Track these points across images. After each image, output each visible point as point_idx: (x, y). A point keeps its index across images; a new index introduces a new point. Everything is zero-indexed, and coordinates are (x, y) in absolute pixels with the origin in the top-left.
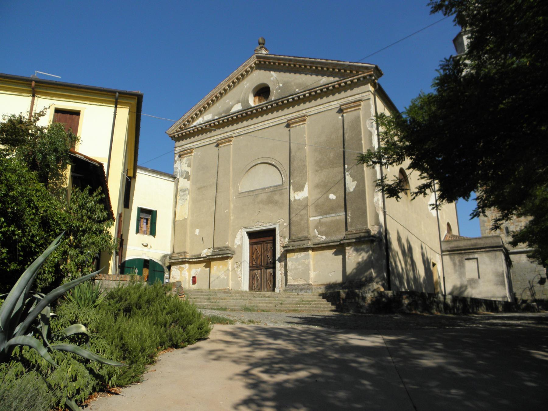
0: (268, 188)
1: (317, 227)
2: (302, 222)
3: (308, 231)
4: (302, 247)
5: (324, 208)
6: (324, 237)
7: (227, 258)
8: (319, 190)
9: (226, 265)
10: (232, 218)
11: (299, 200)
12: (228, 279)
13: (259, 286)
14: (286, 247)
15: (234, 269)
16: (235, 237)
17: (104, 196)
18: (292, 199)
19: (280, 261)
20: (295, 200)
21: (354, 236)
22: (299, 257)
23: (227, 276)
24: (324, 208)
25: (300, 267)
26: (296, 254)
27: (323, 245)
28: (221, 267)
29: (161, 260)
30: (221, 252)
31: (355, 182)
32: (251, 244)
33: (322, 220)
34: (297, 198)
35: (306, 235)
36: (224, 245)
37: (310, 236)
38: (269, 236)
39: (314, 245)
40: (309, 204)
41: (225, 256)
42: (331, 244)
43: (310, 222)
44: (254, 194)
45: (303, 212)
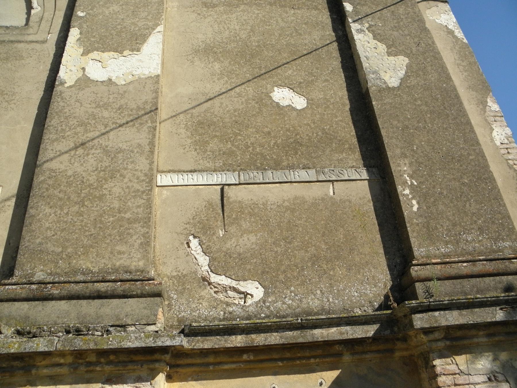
1: (201, 229)
3: (146, 243)
4: (115, 341)
5: (235, 141)
6: (256, 290)
8: (217, 66)
14: (78, 332)
18: (67, 74)
20: (84, 81)
21: (492, 288)
24: (235, 141)
27: (259, 339)
29: (506, 318)
31: (402, 61)
33: (230, 192)
34: (96, 72)
35: (135, 262)
37: (165, 269)
39: (190, 332)
40: (164, 113)
42: (319, 334)
43: (159, 197)
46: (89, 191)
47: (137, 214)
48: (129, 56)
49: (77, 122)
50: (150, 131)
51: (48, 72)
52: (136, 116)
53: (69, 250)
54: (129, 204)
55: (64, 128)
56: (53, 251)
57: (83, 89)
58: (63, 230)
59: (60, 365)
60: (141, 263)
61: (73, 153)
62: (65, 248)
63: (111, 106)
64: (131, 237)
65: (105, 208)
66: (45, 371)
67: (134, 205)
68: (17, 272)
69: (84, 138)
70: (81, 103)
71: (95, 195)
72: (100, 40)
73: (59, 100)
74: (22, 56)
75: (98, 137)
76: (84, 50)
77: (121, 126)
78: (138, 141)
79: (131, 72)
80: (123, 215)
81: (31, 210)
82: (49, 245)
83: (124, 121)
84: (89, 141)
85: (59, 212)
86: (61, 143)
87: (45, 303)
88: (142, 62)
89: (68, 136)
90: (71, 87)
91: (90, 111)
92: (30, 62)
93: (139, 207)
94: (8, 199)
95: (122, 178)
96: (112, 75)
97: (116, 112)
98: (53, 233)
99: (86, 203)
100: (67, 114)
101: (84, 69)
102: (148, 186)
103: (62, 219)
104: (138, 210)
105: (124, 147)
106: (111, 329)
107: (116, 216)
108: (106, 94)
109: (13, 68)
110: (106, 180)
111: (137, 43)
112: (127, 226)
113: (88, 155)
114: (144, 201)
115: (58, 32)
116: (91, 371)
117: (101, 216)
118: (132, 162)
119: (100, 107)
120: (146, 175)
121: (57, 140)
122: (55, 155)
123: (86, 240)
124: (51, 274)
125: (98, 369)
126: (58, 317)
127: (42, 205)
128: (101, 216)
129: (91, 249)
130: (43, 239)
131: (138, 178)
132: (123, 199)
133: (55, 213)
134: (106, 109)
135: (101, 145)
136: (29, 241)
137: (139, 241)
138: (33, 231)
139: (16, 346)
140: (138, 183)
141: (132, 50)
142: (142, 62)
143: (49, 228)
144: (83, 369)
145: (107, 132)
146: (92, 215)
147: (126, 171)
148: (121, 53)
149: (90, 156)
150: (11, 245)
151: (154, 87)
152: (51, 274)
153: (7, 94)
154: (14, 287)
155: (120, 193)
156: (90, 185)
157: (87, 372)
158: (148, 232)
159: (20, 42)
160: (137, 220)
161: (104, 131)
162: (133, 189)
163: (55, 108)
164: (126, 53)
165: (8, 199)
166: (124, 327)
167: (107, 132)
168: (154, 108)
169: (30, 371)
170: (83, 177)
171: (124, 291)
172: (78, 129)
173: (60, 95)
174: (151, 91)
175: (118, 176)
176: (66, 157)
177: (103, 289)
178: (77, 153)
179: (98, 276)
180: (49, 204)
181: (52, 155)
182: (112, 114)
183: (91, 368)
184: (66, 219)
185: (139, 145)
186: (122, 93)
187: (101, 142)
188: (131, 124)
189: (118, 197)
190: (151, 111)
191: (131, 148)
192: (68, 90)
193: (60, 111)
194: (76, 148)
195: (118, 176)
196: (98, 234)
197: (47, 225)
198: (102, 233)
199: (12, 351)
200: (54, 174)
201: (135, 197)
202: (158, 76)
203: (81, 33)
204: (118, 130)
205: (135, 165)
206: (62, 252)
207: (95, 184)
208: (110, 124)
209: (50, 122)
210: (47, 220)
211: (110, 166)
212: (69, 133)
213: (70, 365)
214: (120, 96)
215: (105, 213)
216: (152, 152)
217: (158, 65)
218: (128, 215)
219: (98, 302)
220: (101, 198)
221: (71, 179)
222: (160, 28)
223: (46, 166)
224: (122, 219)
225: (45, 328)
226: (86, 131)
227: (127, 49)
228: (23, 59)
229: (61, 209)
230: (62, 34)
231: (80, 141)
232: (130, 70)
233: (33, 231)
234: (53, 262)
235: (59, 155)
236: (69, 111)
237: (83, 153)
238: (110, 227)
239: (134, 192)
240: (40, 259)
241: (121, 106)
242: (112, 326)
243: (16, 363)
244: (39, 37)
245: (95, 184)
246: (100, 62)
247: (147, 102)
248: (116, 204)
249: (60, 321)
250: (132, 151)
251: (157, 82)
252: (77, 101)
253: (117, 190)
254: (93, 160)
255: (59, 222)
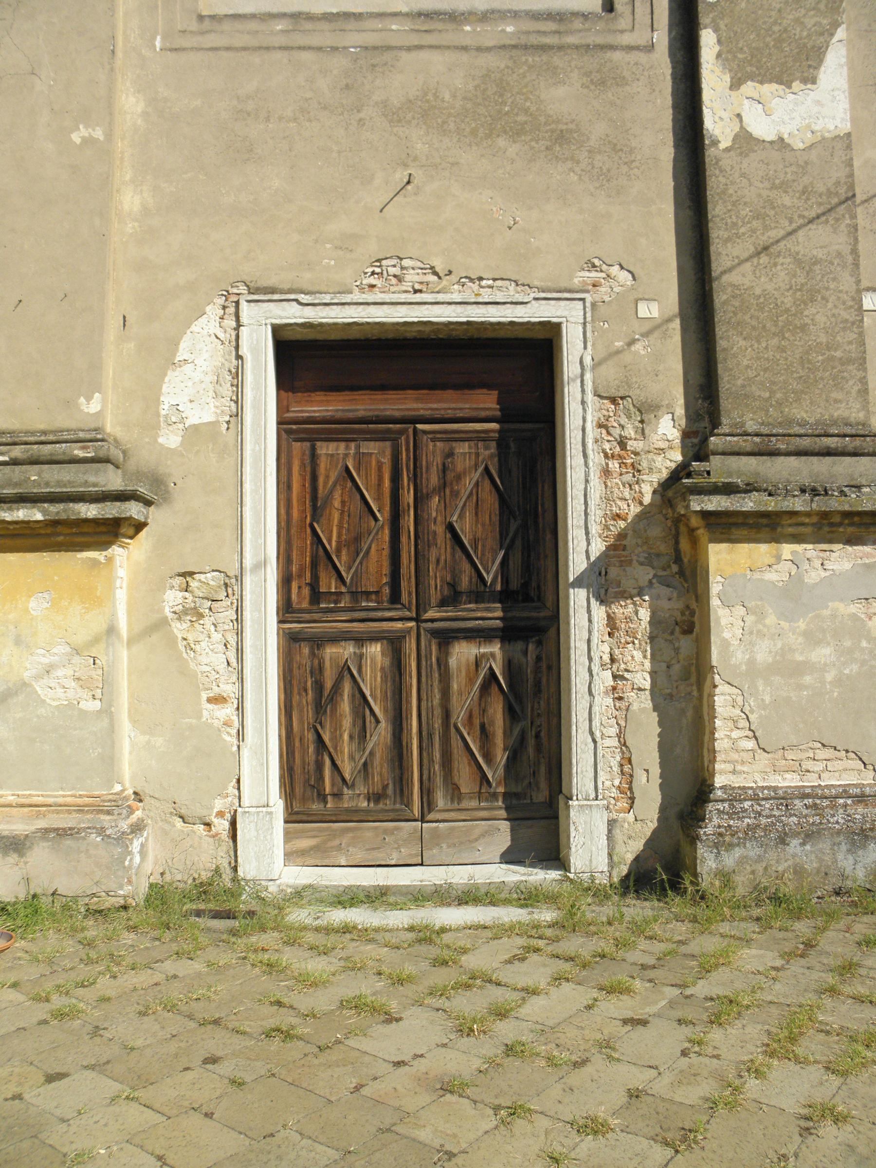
0: (485, 17)
2: (818, 316)
7: (110, 531)
9: (94, 598)
10: (130, 201)
11: (781, 143)
12: (108, 712)
13: (381, 771)
14: (814, 492)
15: (164, 622)
16: (163, 356)
17: (99, 134)
18: (716, 123)
19: (604, 582)
20: (745, 140)
22: (814, 576)
23: (105, 688)
25: (824, 654)
26: (787, 549)
28: (37, 605)
30: (36, 478)
32: (289, 429)
34: (762, 128)
36: (62, 421)
38: (469, 386)
41: (90, 511)
44: (354, 39)
45: (821, 240)
46: (787, 318)
47: (849, 352)
48: (801, 93)
49: (751, 211)
50: (850, 233)
51: (671, 111)
52: (829, 207)
53: (779, 395)
54: (838, 338)
55: (735, 220)
56: (759, 396)
57: (747, 155)
58: (766, 370)
59: (803, 524)
60: (861, 415)
61: (755, 260)
62: (773, 393)
63: (791, 187)
64: (847, 381)
65: (810, 343)
66: (791, 530)
67: (845, 340)
68: (724, 420)
69: (765, 238)
70: (749, 180)
71: (796, 325)
72: (752, 57)
73: (717, 172)
74: (624, 78)
75: (783, 238)
76: (732, 78)
77: (811, 221)
78: (837, 247)
79: (808, 126)
80: (833, 353)
81: (721, 342)
82: (754, 388)
83: (813, 214)
84: (772, 244)
85: (756, 346)
86: (735, 245)
87: (773, 458)
88: (822, 105)
89: (744, 234)
90: (727, 150)
91: (765, 193)
92: (639, 90)
93: (850, 343)
94: (669, 320)
95: (824, 302)
96: (783, 130)
97: (800, 198)
98: (755, 373)
99: (787, 335)
100: (734, 198)
101: (739, 116)
102: (857, 315)
103: (761, 354)
104: (850, 347)
105: (820, 256)
106: (845, 489)
107: (825, 354)
108: (781, 166)
109: (618, 102)
110: (806, 304)
111: (810, 66)
112: (839, 368)
113: (775, 265)
114: (856, 336)
115: (667, 27)
116: (832, 532)
117: (807, 353)
118: (834, 279)
119: (776, 188)
120: (853, 299)
121: (729, 239)
122: (734, 263)
123: (795, 384)
124: (762, 424)
125: (841, 530)
126: (790, 474)
127: (733, 335)
128: (807, 353)
129: (803, 396)
130: (744, 380)
131: (844, 303)
132: (830, 331)
133: (752, 346)
134: (786, 192)
135: (790, 250)
136: (728, 382)
137: (856, 388)
138: (731, 370)
139: (773, 504)
140: (845, 309)
141: (805, 81)
142: (822, 105)
143: (748, 367)
144: (826, 529)
145: (794, 231)
146: (796, 352)
147: (828, 293)
148: (790, 87)
149: (779, 267)
150: (691, 382)
151: (846, 155)
152: (762, 424)
153: (622, 150)
154: (735, 439)
155: (825, 323)
156: (787, 310)
157: (829, 532)
158: (865, 377)
159: (612, 47)
160: (850, 361)
161: (789, 229)
162: (840, 319)
163: (715, 186)
164: (796, 85)
165: (669, 320)
166: (858, 487)
167: (794, 231)
168: (850, 194)
169: (776, 529)
170: (776, 298)
171: (855, 448)
172: (754, 223)
173: (717, 163)
174: (843, 162)
175: (819, 299)
176: (748, 265)
177: (832, 446)
178: (761, 261)
179: (816, 429)
180: (742, 334)
181: (729, 264)
182: (795, 201)
183: (834, 529)
184: (766, 356)
185: (839, 254)
186: (802, 164)
187: (788, 246)
188: (823, 218)
189: (824, 328)
190: (847, 199)
191: (829, 258)
192: (725, 155)
193: (724, 192)
194: (758, 254)
195: (819, 299)
196: (809, 377)
197: (745, 362)
198: (812, 376)
199: (770, 509)
200: (738, 292)
201: (844, 329)
202: (849, 135)
203: (719, 42)
204: (808, 228)
205: (838, 283)
206: (770, 397)
207: (793, 309)
208: (796, 217)
209: (714, 209)
210: (744, 356)
211: (807, 284)
212: (742, 230)
213: (813, 524)
214: (801, 170)
215: (811, 349)
216: (856, 265)
217: (846, 113)
218: (838, 354)
219: (828, 460)
220: (803, 328)
221: (762, 300)
222: (841, 33)
223: (725, 278)
224: (832, 358)
225: (780, 486)
226: (766, 228)
227: (797, 80)
228: (627, 84)
229: (759, 342)
230: (674, 33)
231: (761, 243)
232: (807, 121)
233: (731, 370)
234: (762, 409)
235: (739, 264)
236: (736, 192)
237: (769, 263)
238: (821, 369)
239: (842, 322)
240: (747, 405)
241: (805, 187)
242: (846, 486)
243: (764, 521)
244: (639, 37)
245: (793, 309)
246: (760, 103)
247: (839, 182)
248: (823, 339)
249: (792, 479)
250: (832, 263)
251: (849, 147)
252: (743, 175)
253: (821, 319)
254: (783, 274)
255: (758, 358)
